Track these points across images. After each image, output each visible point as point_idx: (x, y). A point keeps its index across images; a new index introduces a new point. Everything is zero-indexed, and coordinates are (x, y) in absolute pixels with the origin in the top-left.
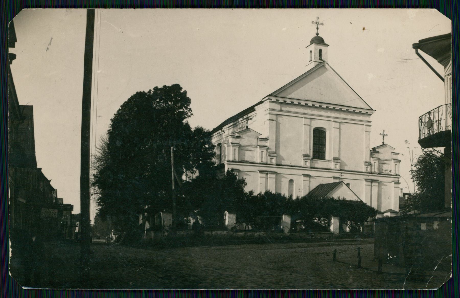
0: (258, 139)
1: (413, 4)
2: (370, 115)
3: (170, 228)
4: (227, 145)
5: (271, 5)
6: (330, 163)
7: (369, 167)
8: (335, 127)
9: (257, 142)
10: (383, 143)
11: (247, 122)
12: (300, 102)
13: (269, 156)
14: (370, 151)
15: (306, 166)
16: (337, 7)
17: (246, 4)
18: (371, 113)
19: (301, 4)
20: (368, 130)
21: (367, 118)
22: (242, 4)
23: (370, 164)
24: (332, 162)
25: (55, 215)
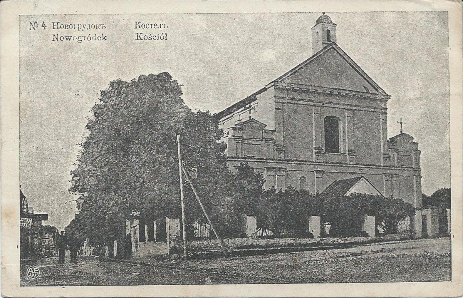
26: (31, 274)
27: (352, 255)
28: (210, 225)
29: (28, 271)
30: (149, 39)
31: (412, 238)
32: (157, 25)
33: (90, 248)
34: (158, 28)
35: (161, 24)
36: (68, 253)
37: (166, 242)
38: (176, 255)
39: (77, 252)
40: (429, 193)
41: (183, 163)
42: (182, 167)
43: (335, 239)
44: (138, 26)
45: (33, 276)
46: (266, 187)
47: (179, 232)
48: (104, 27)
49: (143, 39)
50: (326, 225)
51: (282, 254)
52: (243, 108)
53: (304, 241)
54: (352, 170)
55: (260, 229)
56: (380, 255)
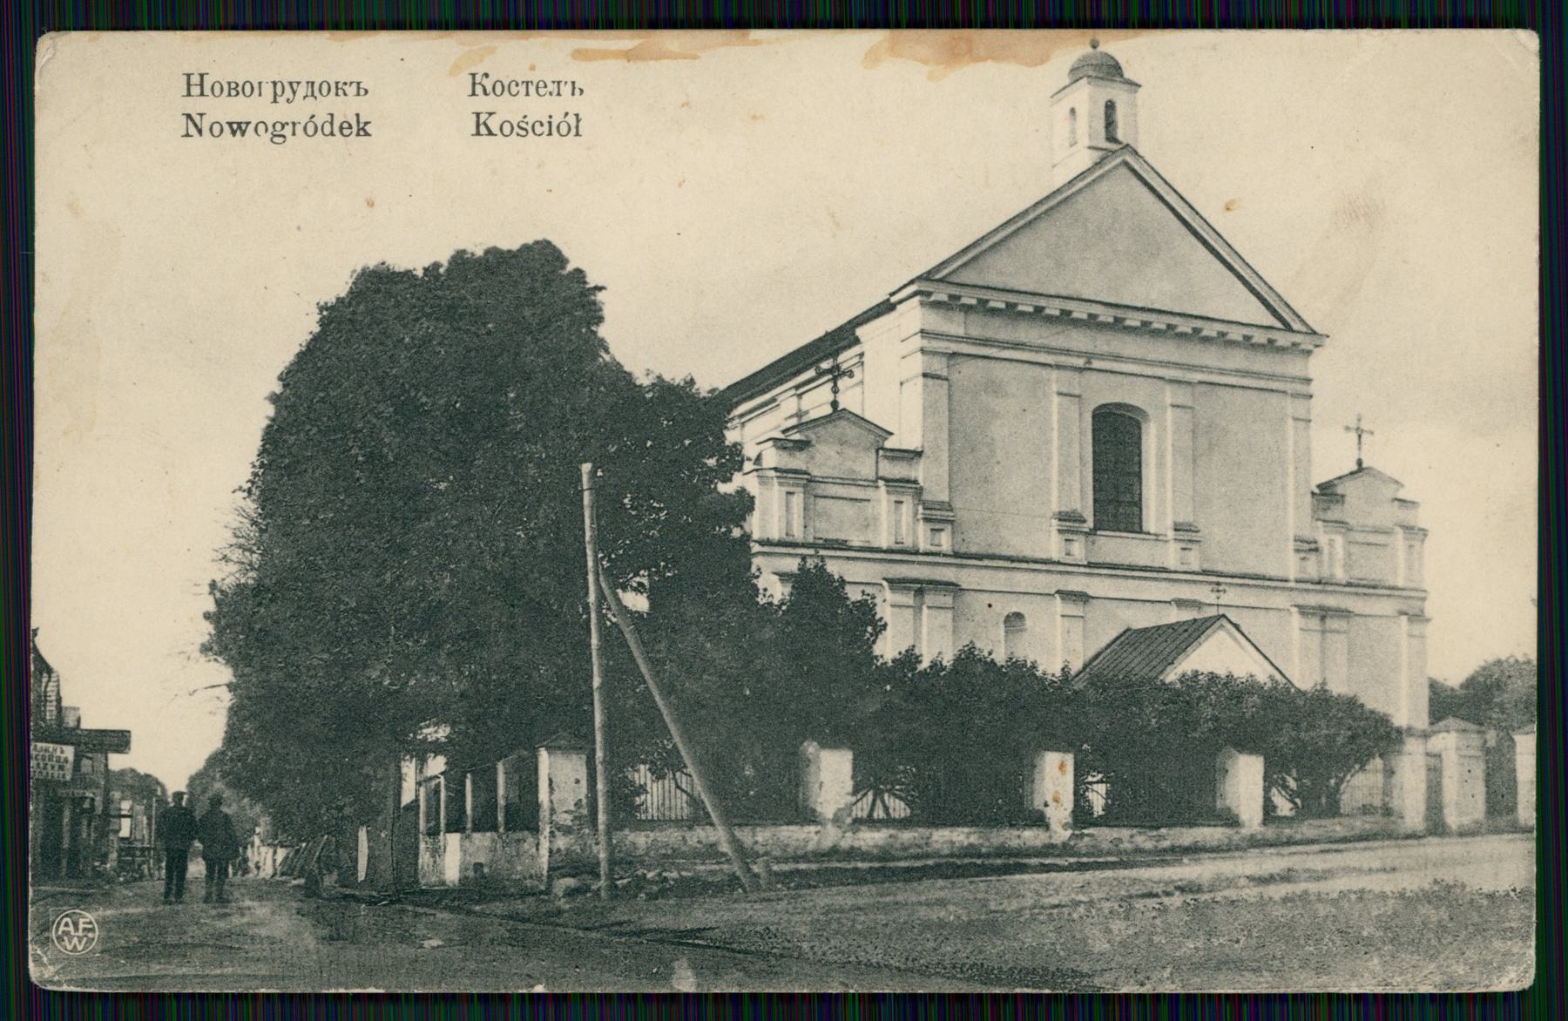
0: (881, 452)
1: (1471, 11)
2: (1309, 352)
3: (576, 818)
4: (758, 476)
5: (980, 16)
6: (1161, 544)
7: (1313, 557)
8: (1175, 402)
9: (877, 462)
10: (1360, 462)
11: (835, 385)
12: (1042, 302)
13: (927, 520)
14: (1313, 494)
15: (1069, 560)
16: (1209, 24)
17: (892, 16)
18: (1310, 347)
19: (1082, 14)
20: (1301, 413)
22: (879, 16)
23: (1313, 546)
24: (1166, 541)
25: (61, 768)
26: (66, 938)
27: (1181, 889)
28: (693, 780)
29: (57, 929)
30: (518, 135)
31: (1388, 835)
32: (546, 87)
33: (275, 853)
34: (551, 94)
35: (559, 83)
36: (196, 869)
37: (535, 830)
38: (570, 882)
39: (230, 867)
40: (1454, 675)
41: (602, 558)
42: (597, 574)
43: (1125, 833)
44: (479, 89)
45: (75, 947)
46: (887, 649)
47: (584, 801)
48: (362, 92)
49: (498, 132)
50: (1091, 783)
51: (941, 883)
52: (811, 373)
53: (1017, 841)
54: (1186, 592)
55: (865, 794)
56: (1277, 891)
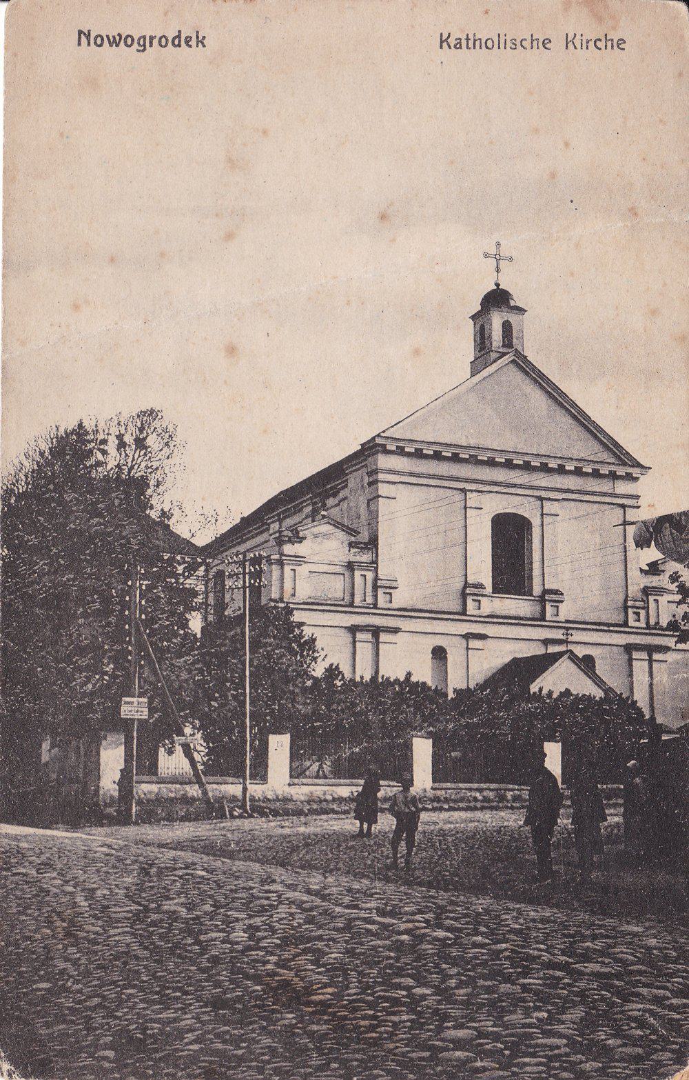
21: (622, 487)
